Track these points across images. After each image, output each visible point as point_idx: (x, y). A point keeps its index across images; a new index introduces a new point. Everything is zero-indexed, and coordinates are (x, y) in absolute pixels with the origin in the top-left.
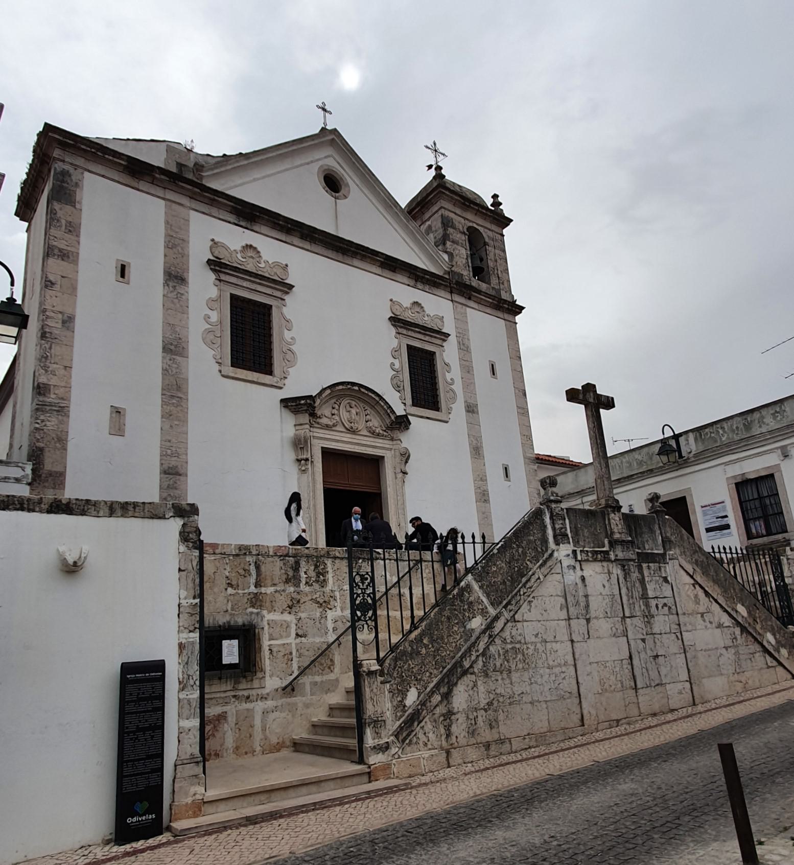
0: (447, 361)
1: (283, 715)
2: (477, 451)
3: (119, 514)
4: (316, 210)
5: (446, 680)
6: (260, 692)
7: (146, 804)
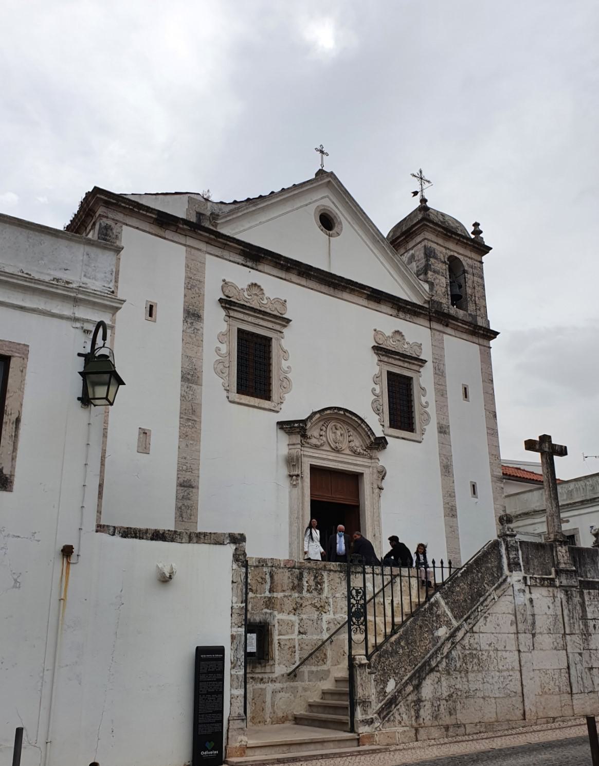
0: (423, 386)
1: (287, 695)
2: (447, 469)
3: (195, 541)
4: (310, 248)
5: (417, 675)
6: (271, 676)
7: (213, 744)
